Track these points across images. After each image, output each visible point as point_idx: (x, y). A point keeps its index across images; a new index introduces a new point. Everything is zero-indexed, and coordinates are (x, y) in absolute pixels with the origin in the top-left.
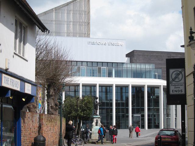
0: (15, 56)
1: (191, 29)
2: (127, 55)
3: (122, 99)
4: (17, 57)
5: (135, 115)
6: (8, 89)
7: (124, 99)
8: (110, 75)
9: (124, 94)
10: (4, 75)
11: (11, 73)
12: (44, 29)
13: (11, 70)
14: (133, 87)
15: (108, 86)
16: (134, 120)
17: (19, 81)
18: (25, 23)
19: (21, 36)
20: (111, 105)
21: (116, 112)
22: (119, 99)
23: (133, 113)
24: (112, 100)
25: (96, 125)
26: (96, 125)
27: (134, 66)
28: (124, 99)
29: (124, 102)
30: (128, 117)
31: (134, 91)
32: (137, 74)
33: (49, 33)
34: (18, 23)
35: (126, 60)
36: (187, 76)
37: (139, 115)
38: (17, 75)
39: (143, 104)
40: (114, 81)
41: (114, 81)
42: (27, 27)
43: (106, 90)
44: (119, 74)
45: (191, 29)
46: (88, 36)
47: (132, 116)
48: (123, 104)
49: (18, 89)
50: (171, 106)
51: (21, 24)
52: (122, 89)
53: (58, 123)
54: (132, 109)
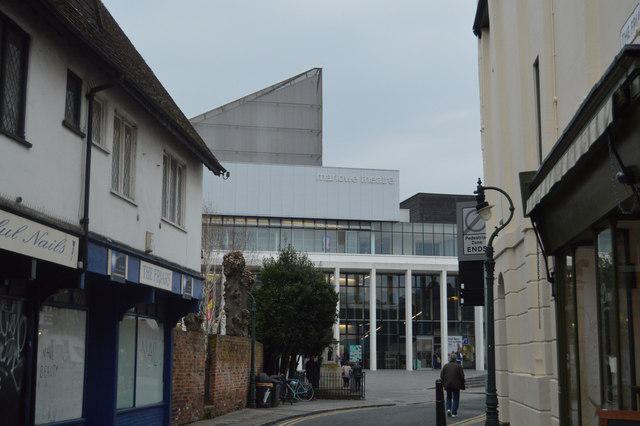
0: (163, 225)
1: (480, 182)
2: (403, 205)
3: (391, 298)
4: (168, 226)
5: (419, 338)
6: (149, 288)
7: (396, 301)
8: (364, 249)
9: (395, 291)
10: (143, 263)
11: (156, 258)
12: (218, 170)
13: (157, 252)
14: (415, 274)
15: (360, 273)
16: (419, 349)
17: (171, 272)
18: (182, 160)
19: (175, 180)
20: (367, 313)
21: (378, 357)
22: (385, 300)
23: (415, 332)
24: (368, 303)
25: (329, 359)
26: (329, 359)
27: (418, 228)
28: (396, 301)
29: (397, 307)
30: (404, 341)
31: (418, 285)
32: (425, 249)
33: (228, 175)
34: (169, 162)
35: (404, 216)
36: (498, 256)
37: (431, 338)
38: (166, 261)
39: (438, 315)
40: (373, 261)
41: (373, 261)
42: (184, 167)
43: (357, 280)
44: (384, 248)
45: (480, 182)
46: (316, 158)
47: (414, 340)
48: (393, 313)
49: (169, 288)
50: (476, 308)
51: (174, 163)
52: (390, 277)
53: (248, 355)
54: (415, 325)
